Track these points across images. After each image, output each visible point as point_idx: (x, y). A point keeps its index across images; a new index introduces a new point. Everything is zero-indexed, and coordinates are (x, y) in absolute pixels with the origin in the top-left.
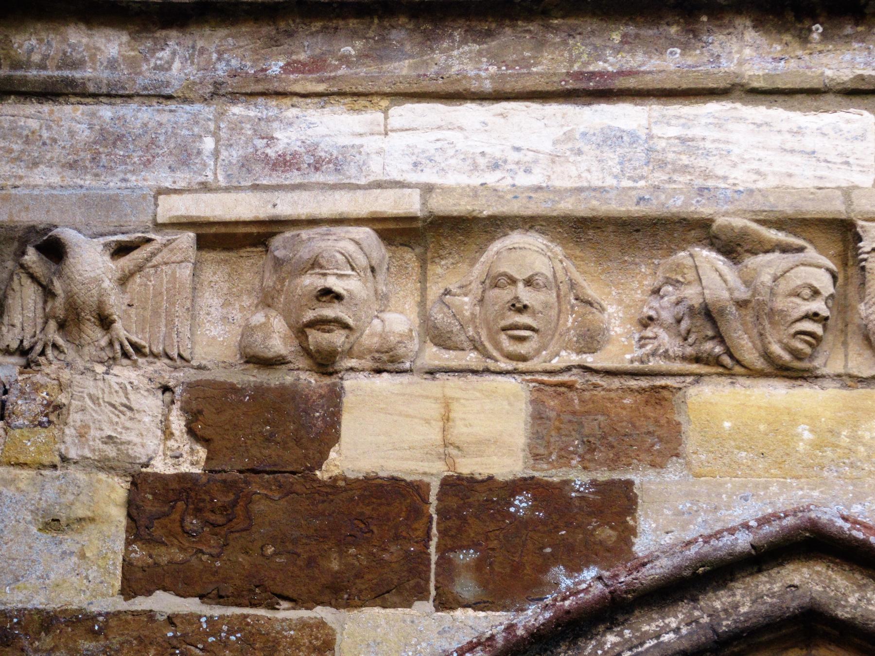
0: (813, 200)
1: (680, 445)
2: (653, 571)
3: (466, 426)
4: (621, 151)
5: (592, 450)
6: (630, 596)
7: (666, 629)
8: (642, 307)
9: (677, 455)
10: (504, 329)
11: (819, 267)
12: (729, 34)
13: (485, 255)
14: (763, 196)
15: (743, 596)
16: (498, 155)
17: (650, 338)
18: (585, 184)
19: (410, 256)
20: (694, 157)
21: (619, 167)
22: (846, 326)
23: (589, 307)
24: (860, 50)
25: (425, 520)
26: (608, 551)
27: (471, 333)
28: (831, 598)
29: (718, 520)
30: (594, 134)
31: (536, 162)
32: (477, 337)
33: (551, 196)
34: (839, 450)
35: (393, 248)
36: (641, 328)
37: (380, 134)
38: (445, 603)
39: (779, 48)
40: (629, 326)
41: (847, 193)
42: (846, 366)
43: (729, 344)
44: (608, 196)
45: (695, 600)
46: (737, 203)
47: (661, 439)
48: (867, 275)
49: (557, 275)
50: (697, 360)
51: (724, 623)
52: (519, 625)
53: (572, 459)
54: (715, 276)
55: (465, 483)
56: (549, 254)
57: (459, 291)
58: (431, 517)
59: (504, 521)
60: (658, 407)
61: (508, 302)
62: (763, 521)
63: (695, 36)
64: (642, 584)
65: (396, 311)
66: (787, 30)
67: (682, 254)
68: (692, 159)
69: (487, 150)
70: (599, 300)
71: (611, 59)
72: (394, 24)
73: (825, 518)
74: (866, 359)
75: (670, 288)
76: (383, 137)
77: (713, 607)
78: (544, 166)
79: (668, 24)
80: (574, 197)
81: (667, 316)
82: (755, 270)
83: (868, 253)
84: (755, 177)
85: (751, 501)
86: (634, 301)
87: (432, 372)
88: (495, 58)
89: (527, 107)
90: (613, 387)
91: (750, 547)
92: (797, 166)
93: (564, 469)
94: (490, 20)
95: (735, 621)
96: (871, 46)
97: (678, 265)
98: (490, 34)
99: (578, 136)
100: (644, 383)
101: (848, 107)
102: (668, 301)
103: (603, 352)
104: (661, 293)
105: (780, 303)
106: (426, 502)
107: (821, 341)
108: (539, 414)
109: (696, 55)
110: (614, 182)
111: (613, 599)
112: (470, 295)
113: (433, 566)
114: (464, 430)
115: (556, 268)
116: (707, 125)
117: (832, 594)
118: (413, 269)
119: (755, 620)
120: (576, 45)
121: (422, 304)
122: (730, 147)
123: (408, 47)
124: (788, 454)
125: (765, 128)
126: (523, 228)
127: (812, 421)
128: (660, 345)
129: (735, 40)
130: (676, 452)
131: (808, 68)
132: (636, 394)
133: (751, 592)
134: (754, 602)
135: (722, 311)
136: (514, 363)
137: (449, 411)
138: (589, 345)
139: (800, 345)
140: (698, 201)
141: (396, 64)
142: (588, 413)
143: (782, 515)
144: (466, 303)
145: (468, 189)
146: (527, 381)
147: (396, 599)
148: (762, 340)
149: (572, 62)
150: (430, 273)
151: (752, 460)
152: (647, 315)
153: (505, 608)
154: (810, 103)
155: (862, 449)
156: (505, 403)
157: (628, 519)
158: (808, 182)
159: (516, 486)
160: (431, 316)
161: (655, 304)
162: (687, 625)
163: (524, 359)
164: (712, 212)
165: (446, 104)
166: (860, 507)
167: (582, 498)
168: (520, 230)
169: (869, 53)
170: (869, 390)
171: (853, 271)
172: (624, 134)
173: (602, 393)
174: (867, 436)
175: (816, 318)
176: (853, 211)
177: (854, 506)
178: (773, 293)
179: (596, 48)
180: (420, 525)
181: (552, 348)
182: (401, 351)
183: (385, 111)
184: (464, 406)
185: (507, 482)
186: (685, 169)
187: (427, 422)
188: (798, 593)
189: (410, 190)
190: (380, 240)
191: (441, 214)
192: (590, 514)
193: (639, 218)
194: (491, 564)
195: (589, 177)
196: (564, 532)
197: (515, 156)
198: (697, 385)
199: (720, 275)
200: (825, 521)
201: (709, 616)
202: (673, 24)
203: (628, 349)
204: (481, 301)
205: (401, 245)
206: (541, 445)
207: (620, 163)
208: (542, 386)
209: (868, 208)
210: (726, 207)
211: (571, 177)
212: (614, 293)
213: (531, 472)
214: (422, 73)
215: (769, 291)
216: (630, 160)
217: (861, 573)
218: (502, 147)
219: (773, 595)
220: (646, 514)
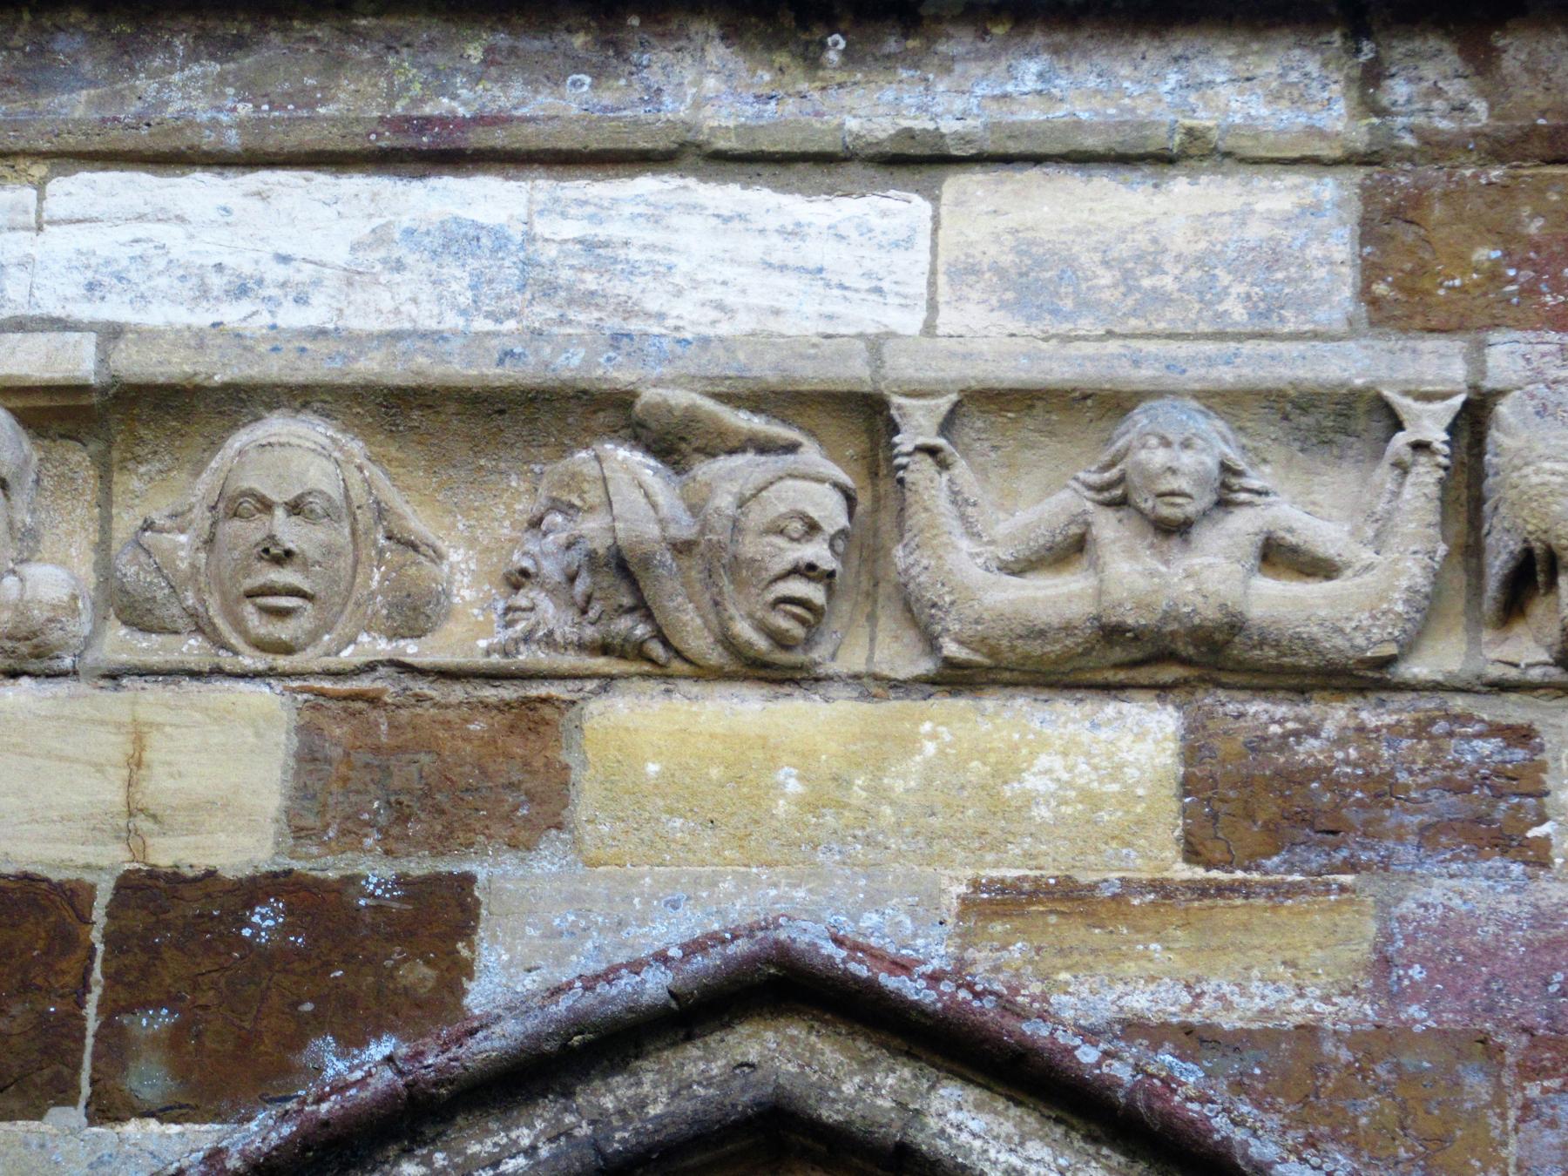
0: (815, 357)
1: (565, 806)
2: (487, 1045)
3: (172, 775)
4: (476, 264)
5: (403, 818)
6: (443, 1091)
7: (512, 1150)
8: (511, 552)
9: (559, 827)
10: (250, 595)
11: (820, 480)
12: (678, 50)
13: (218, 457)
14: (727, 350)
15: (655, 1085)
16: (247, 269)
17: (524, 610)
18: (407, 325)
19: (78, 458)
20: (607, 276)
21: (469, 294)
22: (876, 585)
23: (411, 553)
24: (912, 82)
25: (81, 953)
26: (419, 1006)
27: (190, 602)
28: (812, 1085)
29: (622, 945)
30: (428, 233)
31: (317, 283)
32: (201, 610)
33: (342, 348)
34: (847, 813)
35: (47, 442)
36: (508, 589)
37: (27, 228)
38: (106, 1110)
39: (767, 77)
40: (487, 587)
41: (876, 344)
42: (870, 659)
43: (660, 619)
44: (447, 347)
45: (568, 1094)
46: (680, 363)
47: (531, 797)
48: (908, 494)
49: (352, 494)
50: (605, 649)
51: (618, 1136)
52: (232, 1150)
53: (366, 836)
54: (638, 496)
55: (162, 883)
56: (336, 454)
57: (168, 523)
58: (92, 949)
59: (229, 954)
60: (532, 737)
61: (257, 545)
62: (693, 947)
63: (618, 54)
64: (466, 1068)
65: (52, 561)
66: (783, 45)
67: (583, 454)
68: (603, 280)
69: (227, 260)
70: (432, 538)
71: (464, 92)
72: (61, 23)
73: (803, 940)
74: (907, 646)
75: (559, 518)
76: (33, 234)
77: (600, 1107)
78: (331, 292)
79: (569, 30)
80: (384, 350)
81: (551, 569)
82: (708, 485)
83: (909, 454)
84: (715, 314)
85: (686, 910)
86: (498, 540)
87: (114, 676)
88: (250, 89)
89: (307, 180)
90: (453, 699)
91: (667, 995)
92: (790, 295)
93: (349, 855)
94: (241, 17)
95: (637, 1132)
96: (931, 76)
97: (573, 476)
98: (240, 44)
99: (397, 236)
100: (508, 692)
101: (886, 187)
102: (554, 542)
103: (437, 635)
104: (543, 527)
105: (750, 547)
106: (86, 920)
107: (822, 614)
108: (311, 751)
109: (618, 89)
110: (460, 322)
111: (411, 1097)
112: (190, 531)
113: (89, 1041)
114: (170, 784)
115: (350, 481)
116: (633, 217)
117: (815, 1078)
118: (85, 481)
119: (672, 1130)
120: (400, 66)
121: (103, 546)
122: (673, 259)
123: (87, 66)
124: (756, 822)
125: (737, 225)
126: (290, 406)
127: (805, 757)
128: (538, 623)
129: (689, 60)
130: (556, 820)
131: (818, 114)
132: (494, 712)
133: (670, 1078)
134: (674, 1095)
135: (646, 561)
136: (270, 658)
137: (142, 749)
138: (411, 623)
139: (782, 623)
140: (609, 359)
141: (65, 98)
142: (401, 749)
143: (728, 936)
144: (182, 546)
145: (187, 334)
146: (293, 690)
147: (15, 1104)
148: (718, 614)
149: (392, 97)
150: (117, 489)
151: (692, 833)
152: (518, 566)
153: (218, 1117)
154: (818, 179)
155: (887, 810)
156: (249, 732)
157: (460, 945)
158: (807, 324)
159: (256, 889)
160: (117, 570)
161: (533, 547)
162: (550, 1140)
163: (287, 649)
164: (633, 379)
165: (155, 173)
166: (875, 918)
167: (378, 909)
168: (284, 410)
169: (927, 89)
170: (907, 702)
171: (886, 486)
172: (483, 234)
173: (433, 711)
174: (899, 786)
175: (812, 574)
176: (884, 378)
177: (867, 915)
178: (736, 527)
179: (437, 73)
180: (71, 964)
181: (343, 627)
182: (54, 636)
183: (40, 186)
184: (170, 737)
185: (240, 880)
186: (589, 299)
187: (99, 768)
188: (754, 1077)
189: (77, 335)
190: (19, 428)
191: (134, 380)
192: (390, 938)
193: (503, 389)
194: (198, 1036)
195: (414, 312)
196: (339, 973)
197: (279, 272)
198: (604, 696)
199: (647, 495)
200: (803, 946)
201: (592, 1122)
202: (577, 31)
203: (483, 629)
204: (210, 542)
205: (62, 436)
206: (309, 810)
207: (473, 287)
208: (321, 700)
209: (910, 372)
210: (659, 370)
211: (381, 312)
212: (460, 526)
213: (288, 861)
214: (108, 115)
215: (730, 525)
216: (491, 281)
217: (868, 1039)
218: (255, 255)
219: (708, 1082)
220: (494, 936)
